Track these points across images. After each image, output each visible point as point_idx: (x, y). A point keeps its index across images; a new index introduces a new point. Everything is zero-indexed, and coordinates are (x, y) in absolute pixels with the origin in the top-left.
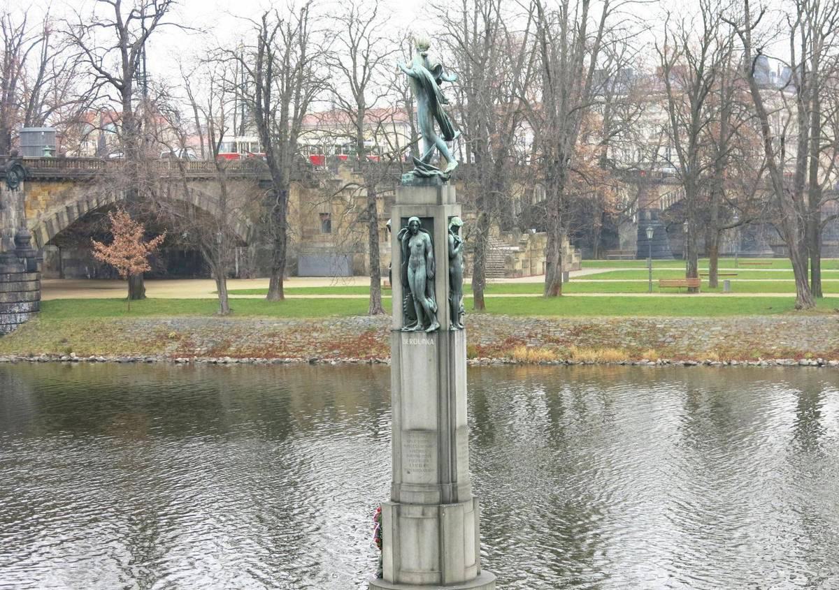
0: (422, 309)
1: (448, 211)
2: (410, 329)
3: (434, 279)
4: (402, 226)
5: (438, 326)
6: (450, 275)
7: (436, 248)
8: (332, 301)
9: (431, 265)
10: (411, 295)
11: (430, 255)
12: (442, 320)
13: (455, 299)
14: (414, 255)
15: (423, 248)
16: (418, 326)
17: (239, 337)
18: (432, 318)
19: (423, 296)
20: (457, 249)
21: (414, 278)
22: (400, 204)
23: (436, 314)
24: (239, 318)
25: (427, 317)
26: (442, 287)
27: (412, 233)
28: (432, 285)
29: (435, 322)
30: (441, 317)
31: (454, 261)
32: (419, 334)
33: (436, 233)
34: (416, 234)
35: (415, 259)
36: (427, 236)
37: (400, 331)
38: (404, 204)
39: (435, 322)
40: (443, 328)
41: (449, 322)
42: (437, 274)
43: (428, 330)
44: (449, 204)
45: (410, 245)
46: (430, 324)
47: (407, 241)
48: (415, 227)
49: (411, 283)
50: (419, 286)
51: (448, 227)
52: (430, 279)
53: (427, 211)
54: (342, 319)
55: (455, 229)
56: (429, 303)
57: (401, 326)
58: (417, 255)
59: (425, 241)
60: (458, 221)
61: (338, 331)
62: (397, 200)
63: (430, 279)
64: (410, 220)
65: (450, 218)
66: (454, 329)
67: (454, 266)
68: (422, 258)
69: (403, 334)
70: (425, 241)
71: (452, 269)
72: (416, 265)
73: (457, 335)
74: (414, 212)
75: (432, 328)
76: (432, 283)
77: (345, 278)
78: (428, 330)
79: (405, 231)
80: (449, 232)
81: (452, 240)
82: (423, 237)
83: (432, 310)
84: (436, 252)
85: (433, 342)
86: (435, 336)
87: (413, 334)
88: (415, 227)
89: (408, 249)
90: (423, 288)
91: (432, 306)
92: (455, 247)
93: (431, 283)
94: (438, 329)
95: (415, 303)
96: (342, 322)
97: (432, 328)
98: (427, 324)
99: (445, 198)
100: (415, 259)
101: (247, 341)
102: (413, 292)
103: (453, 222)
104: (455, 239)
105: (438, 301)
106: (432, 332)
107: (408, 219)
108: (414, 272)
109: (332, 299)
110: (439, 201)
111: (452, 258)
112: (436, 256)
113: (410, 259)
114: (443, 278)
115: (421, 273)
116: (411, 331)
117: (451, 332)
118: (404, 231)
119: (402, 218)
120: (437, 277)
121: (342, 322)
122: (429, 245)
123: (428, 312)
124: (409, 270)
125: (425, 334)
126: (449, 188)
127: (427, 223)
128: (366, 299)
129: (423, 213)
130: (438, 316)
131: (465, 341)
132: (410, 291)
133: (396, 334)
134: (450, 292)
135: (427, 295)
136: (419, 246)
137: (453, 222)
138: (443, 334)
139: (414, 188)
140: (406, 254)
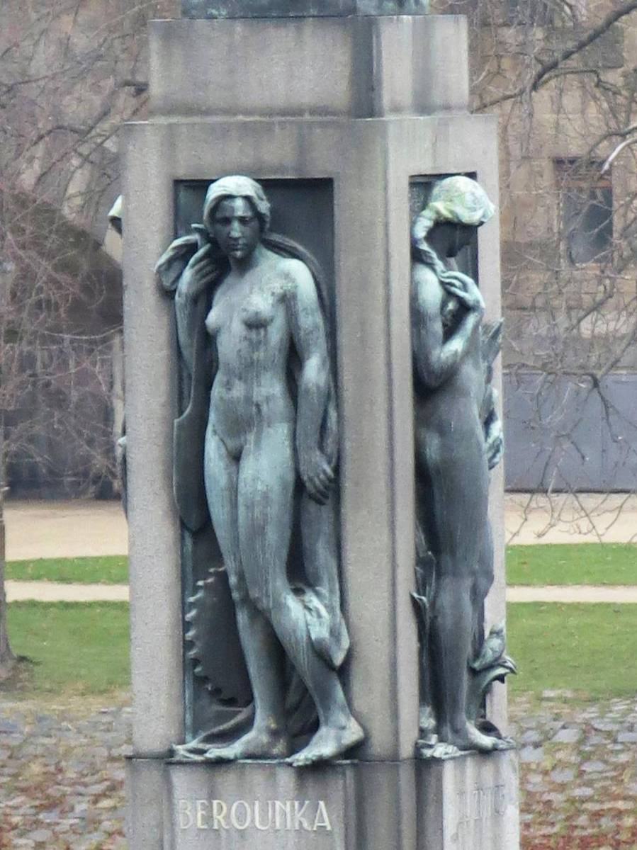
0: (278, 652)
1: (405, 148)
2: (215, 752)
3: (332, 492)
4: (179, 222)
5: (353, 733)
6: (423, 474)
7: (344, 339)
8: (554, 620)
9: (321, 426)
10: (224, 577)
11: (313, 371)
12: (383, 701)
13: (446, 599)
14: (230, 372)
15: (276, 334)
16: (255, 737)
17: (51, 804)
18: (326, 696)
19: (279, 582)
20: (457, 344)
21: (233, 489)
22: (170, 110)
23: (343, 672)
24: (55, 706)
25: (306, 684)
26: (379, 534)
27: (224, 262)
28: (326, 528)
29: (341, 717)
30: (369, 689)
31: (443, 407)
32: (257, 778)
33: (346, 263)
34: (246, 264)
35: (238, 391)
36: (298, 274)
37: (167, 759)
38: (189, 110)
39: (341, 717)
40: (379, 745)
41: (413, 715)
42: (349, 469)
43: (303, 756)
44: (423, 107)
45: (213, 318)
46: (314, 727)
47: (204, 298)
48: (236, 230)
49: (219, 512)
50: (258, 531)
51: (402, 226)
52: (315, 498)
53: (303, 148)
54: (591, 713)
55: (454, 238)
56: (306, 617)
57: (173, 732)
58: (249, 370)
59: (287, 300)
60: (470, 200)
61: (567, 776)
62: (156, 89)
63: (315, 498)
64: (214, 191)
65: (423, 185)
66: (440, 750)
67: (442, 430)
68: (271, 388)
69: (180, 778)
70: (287, 300)
71: (433, 449)
72: (244, 423)
73: (458, 785)
74: (235, 151)
75: (323, 745)
76: (326, 512)
77: (590, 501)
78: (303, 756)
79: (191, 248)
80: (417, 257)
81: (431, 292)
82: (282, 277)
83: (320, 653)
84: (345, 359)
85: (327, 815)
86: (341, 785)
87: (227, 780)
88: (236, 230)
89: (207, 340)
90: (275, 538)
91: (320, 632)
92: (450, 331)
93: (319, 517)
94: (354, 752)
95: (242, 618)
96: (587, 730)
97: (323, 745)
98: (299, 721)
99: (396, 76)
100: (238, 391)
101: (91, 823)
102: (230, 565)
103: (440, 206)
104: (449, 294)
105: (361, 607)
106: (320, 767)
107: (204, 185)
108: (236, 457)
109: (556, 607)
110: (365, 100)
111: (431, 387)
112: (347, 376)
113: (217, 391)
114: (381, 485)
115: (267, 466)
116: (220, 762)
117: (424, 766)
118: (185, 253)
119: (178, 183)
120: (348, 485)
121: (587, 730)
122: (311, 320)
123: (303, 660)
124: (213, 448)
125: (286, 779)
126: (423, 39)
127: (302, 207)
128: (615, 610)
129: (280, 155)
130: (357, 686)
131: (512, 814)
132: (216, 556)
133: (150, 777)
134: (420, 562)
135: (300, 574)
136: (256, 324)
137: (440, 206)
138: (381, 778)
139: (239, 27)
140: (196, 366)
